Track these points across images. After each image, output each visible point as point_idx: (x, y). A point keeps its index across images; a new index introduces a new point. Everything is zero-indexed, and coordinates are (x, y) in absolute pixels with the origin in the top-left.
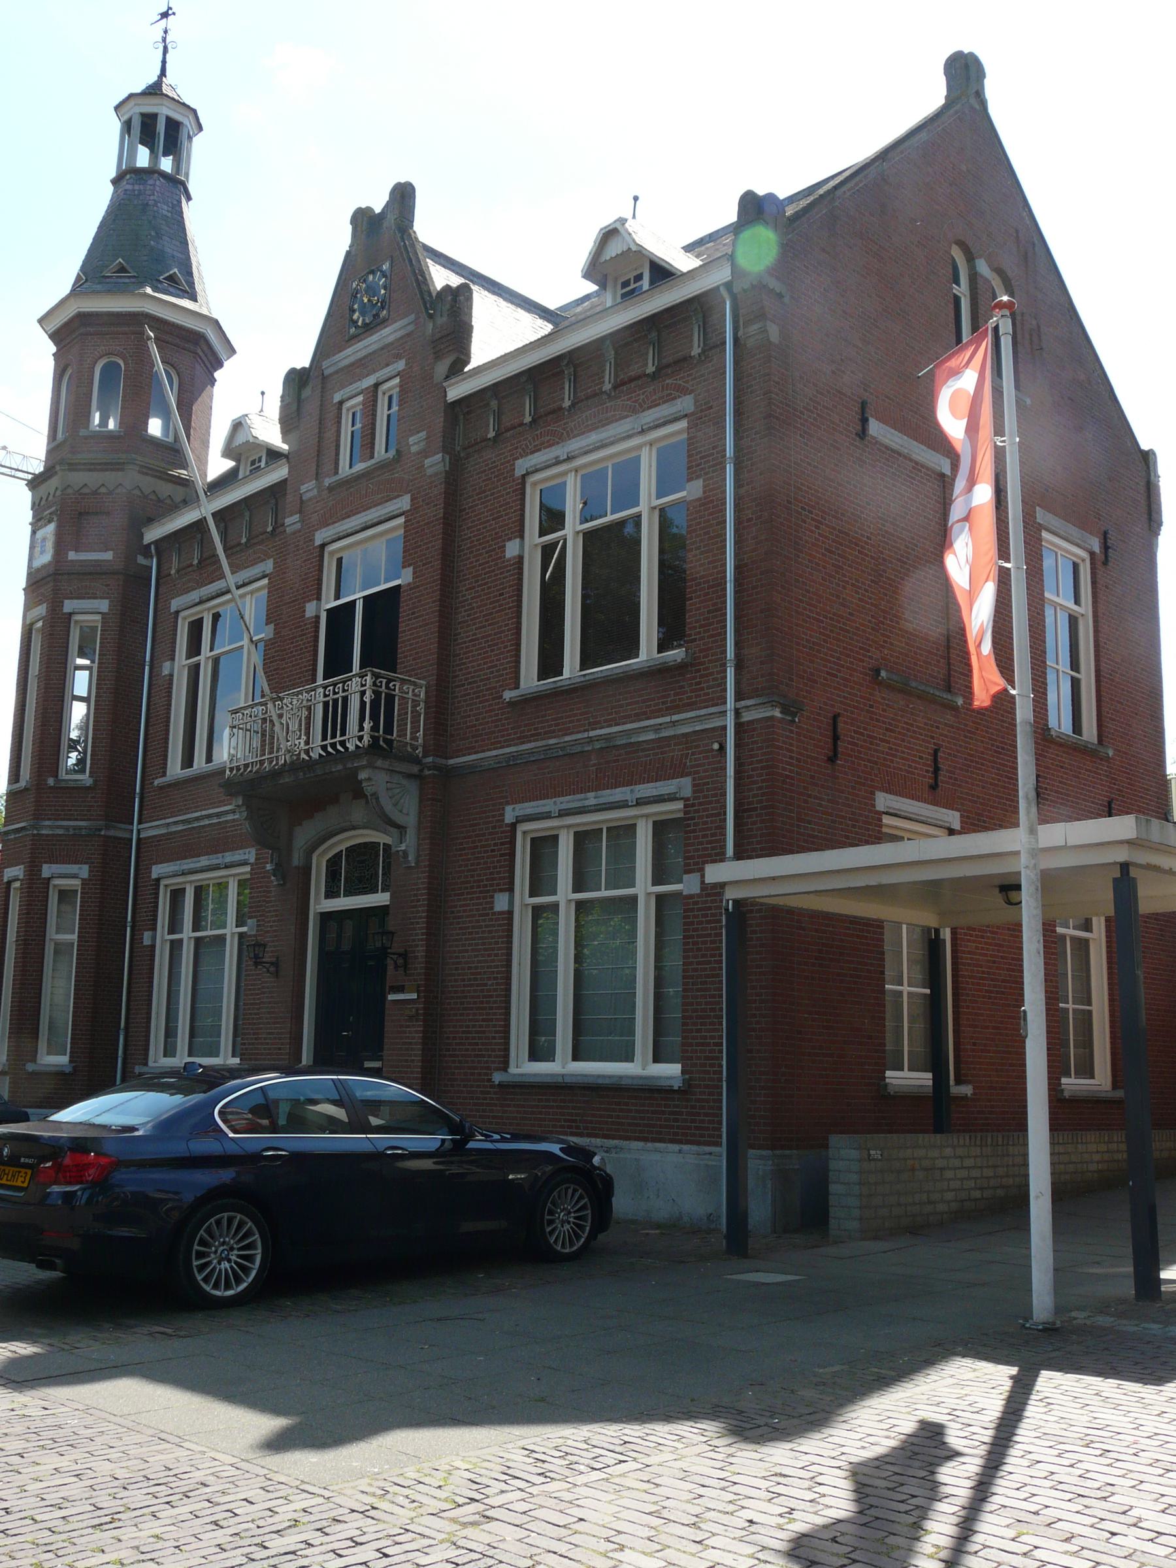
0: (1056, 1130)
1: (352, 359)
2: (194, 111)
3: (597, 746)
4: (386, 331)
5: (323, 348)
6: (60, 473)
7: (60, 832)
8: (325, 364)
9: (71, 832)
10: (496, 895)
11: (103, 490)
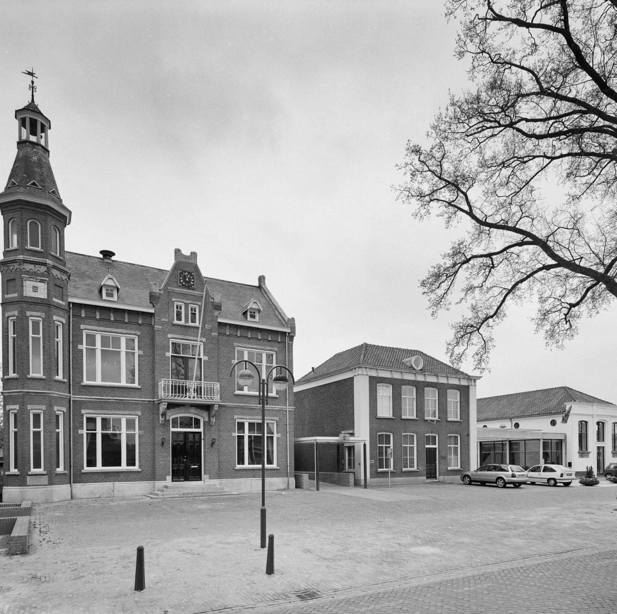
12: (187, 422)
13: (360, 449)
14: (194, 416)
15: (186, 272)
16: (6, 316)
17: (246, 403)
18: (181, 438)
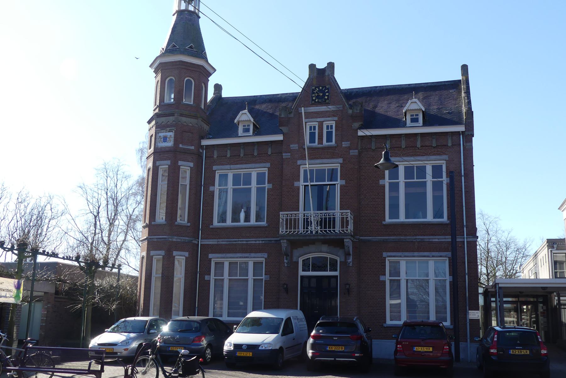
1: (313, 111)
12: (319, 265)
14: (329, 256)
15: (321, 80)
18: (313, 283)
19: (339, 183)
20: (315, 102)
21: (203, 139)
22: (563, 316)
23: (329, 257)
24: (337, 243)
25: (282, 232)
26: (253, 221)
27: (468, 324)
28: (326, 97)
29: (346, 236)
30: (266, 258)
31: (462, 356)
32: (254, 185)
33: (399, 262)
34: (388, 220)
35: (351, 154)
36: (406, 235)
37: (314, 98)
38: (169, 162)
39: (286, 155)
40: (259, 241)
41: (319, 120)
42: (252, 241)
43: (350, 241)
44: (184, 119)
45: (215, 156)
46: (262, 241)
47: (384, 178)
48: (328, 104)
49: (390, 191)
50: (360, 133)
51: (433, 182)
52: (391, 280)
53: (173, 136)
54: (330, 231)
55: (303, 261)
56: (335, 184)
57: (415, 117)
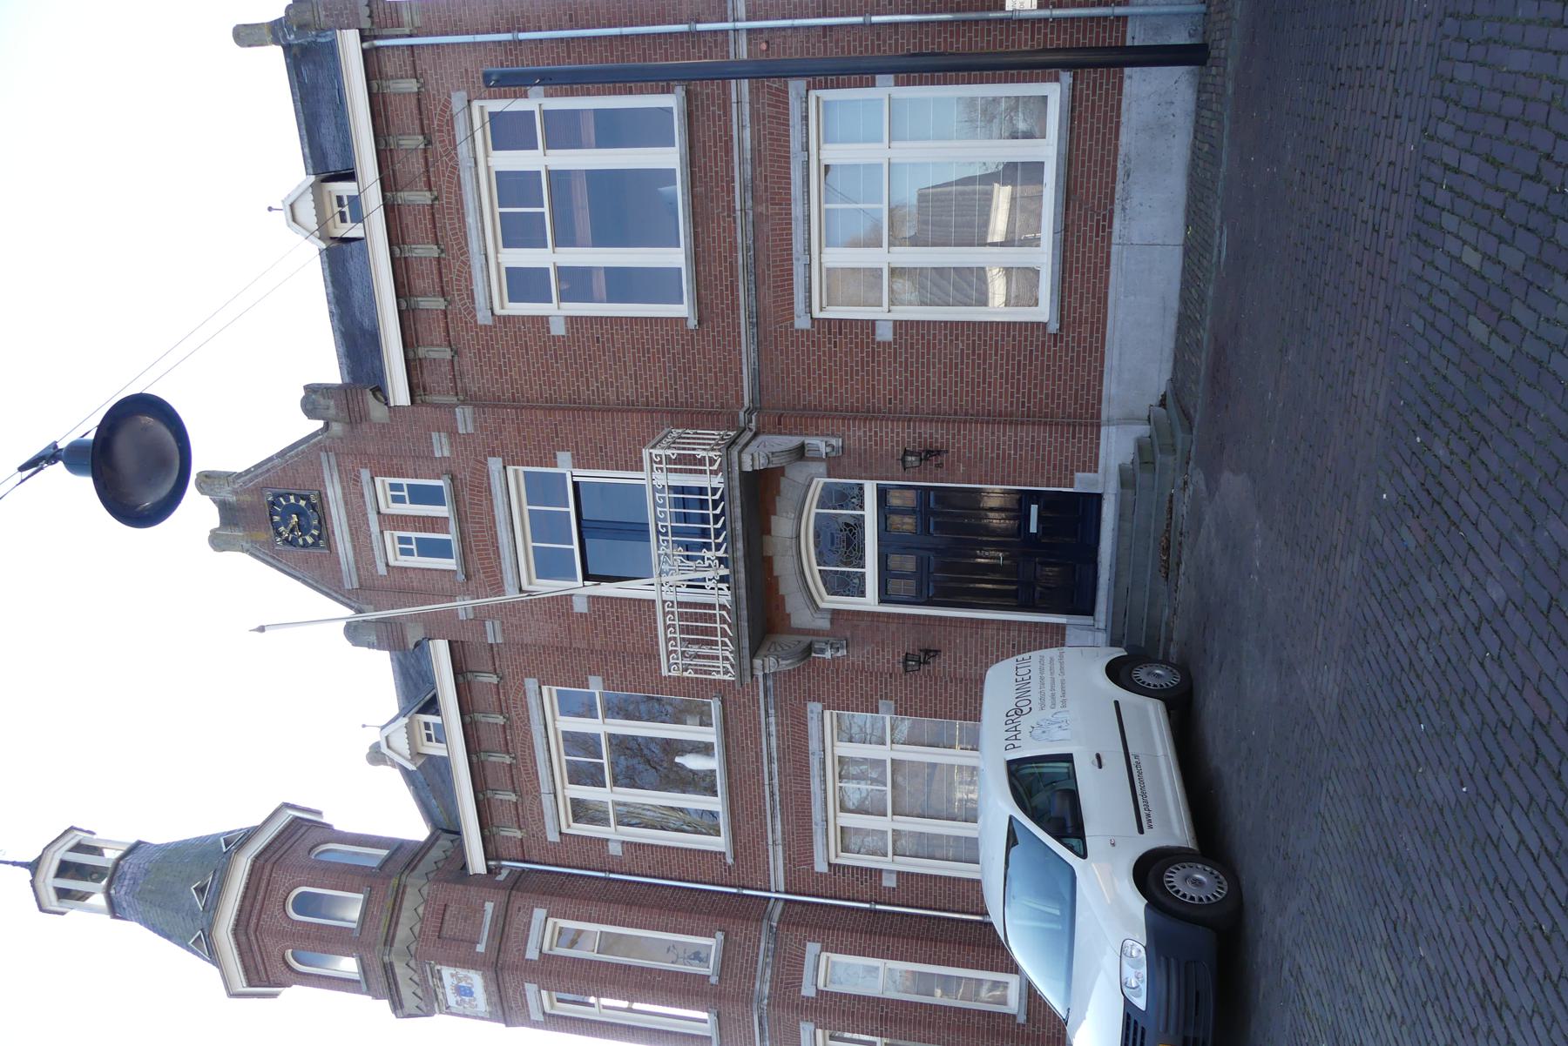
0: (1063, 638)
1: (349, 545)
2: (72, 828)
3: (749, 203)
4: (330, 493)
5: (327, 581)
6: (393, 958)
7: (769, 972)
8: (348, 586)
9: (769, 960)
10: (878, 339)
11: (421, 910)
12: (842, 542)
13: (913, 972)
14: (812, 510)
16: (541, 1018)
17: (732, 269)
19: (565, 467)
20: (319, 537)
21: (464, 867)
22: (1164, 773)
23: (814, 510)
24: (759, 493)
25: (726, 672)
26: (710, 735)
27: (1058, 12)
28: (302, 503)
29: (729, 464)
30: (824, 708)
31: (1180, 37)
32: (600, 726)
33: (828, 270)
34: (682, 309)
35: (471, 429)
36: (733, 248)
37: (310, 540)
38: (531, 989)
39: (493, 633)
40: (767, 725)
41: (374, 527)
42: (771, 742)
43: (752, 448)
44: (402, 933)
45: (519, 834)
46: (767, 715)
47: (543, 320)
48: (322, 497)
49: (588, 297)
50: (400, 393)
51: (550, 145)
52: (892, 302)
53: (452, 970)
54: (717, 518)
55: (831, 592)
56: (576, 485)
57: (346, 209)
